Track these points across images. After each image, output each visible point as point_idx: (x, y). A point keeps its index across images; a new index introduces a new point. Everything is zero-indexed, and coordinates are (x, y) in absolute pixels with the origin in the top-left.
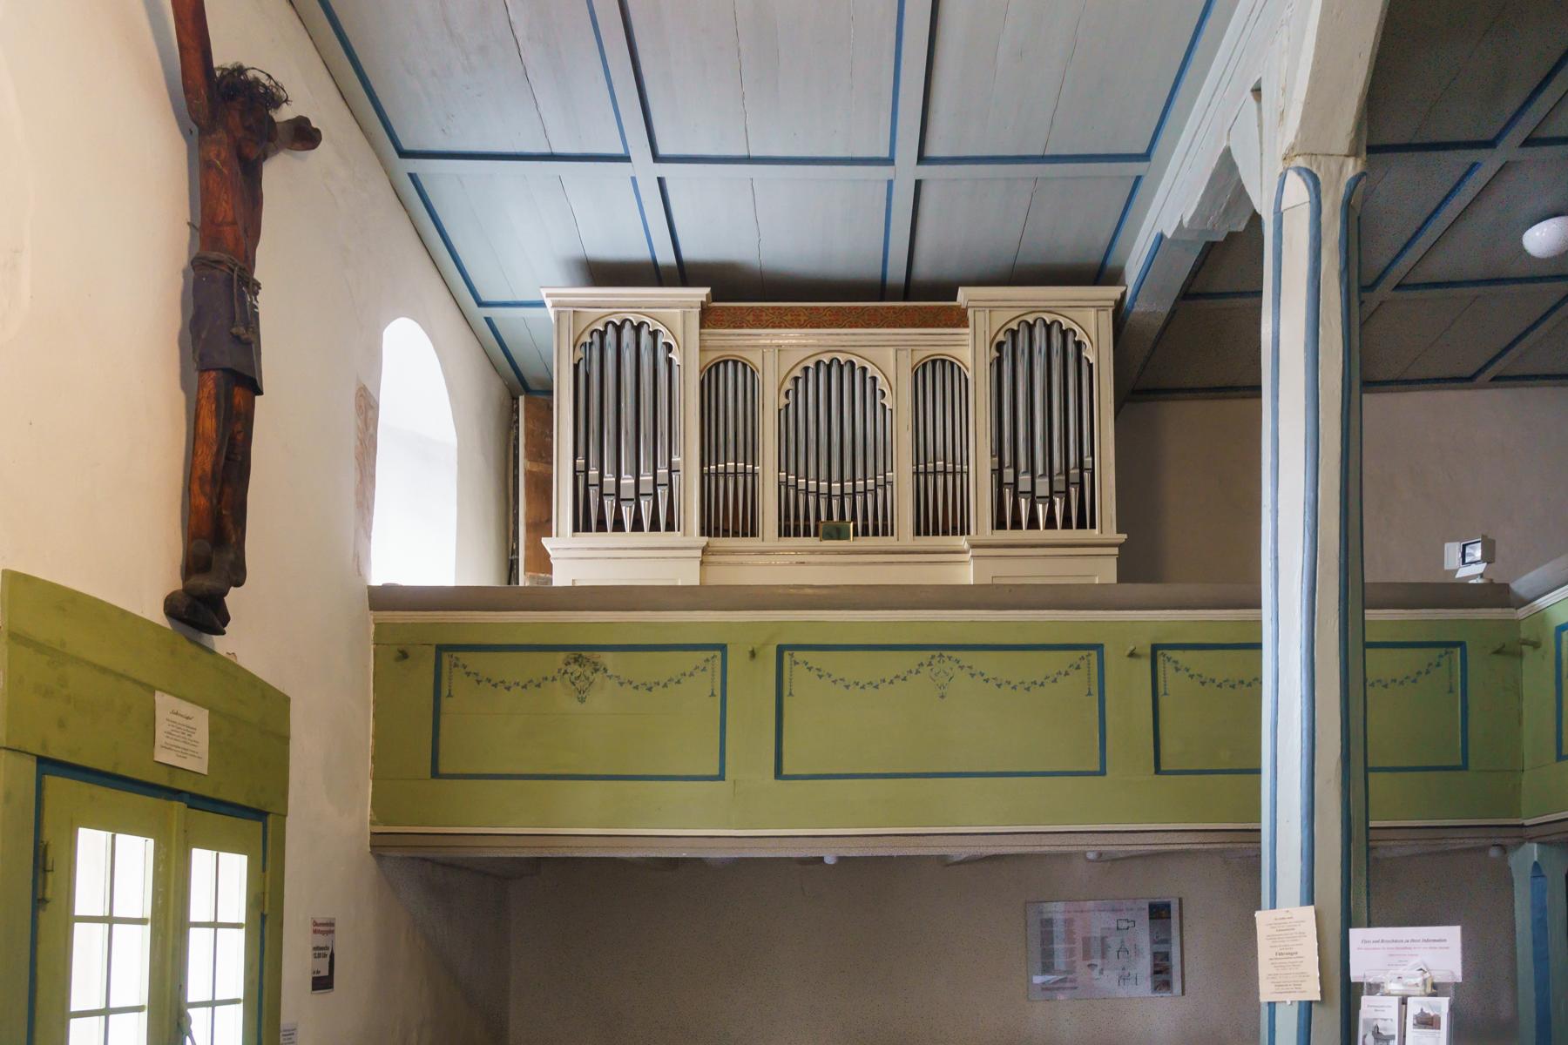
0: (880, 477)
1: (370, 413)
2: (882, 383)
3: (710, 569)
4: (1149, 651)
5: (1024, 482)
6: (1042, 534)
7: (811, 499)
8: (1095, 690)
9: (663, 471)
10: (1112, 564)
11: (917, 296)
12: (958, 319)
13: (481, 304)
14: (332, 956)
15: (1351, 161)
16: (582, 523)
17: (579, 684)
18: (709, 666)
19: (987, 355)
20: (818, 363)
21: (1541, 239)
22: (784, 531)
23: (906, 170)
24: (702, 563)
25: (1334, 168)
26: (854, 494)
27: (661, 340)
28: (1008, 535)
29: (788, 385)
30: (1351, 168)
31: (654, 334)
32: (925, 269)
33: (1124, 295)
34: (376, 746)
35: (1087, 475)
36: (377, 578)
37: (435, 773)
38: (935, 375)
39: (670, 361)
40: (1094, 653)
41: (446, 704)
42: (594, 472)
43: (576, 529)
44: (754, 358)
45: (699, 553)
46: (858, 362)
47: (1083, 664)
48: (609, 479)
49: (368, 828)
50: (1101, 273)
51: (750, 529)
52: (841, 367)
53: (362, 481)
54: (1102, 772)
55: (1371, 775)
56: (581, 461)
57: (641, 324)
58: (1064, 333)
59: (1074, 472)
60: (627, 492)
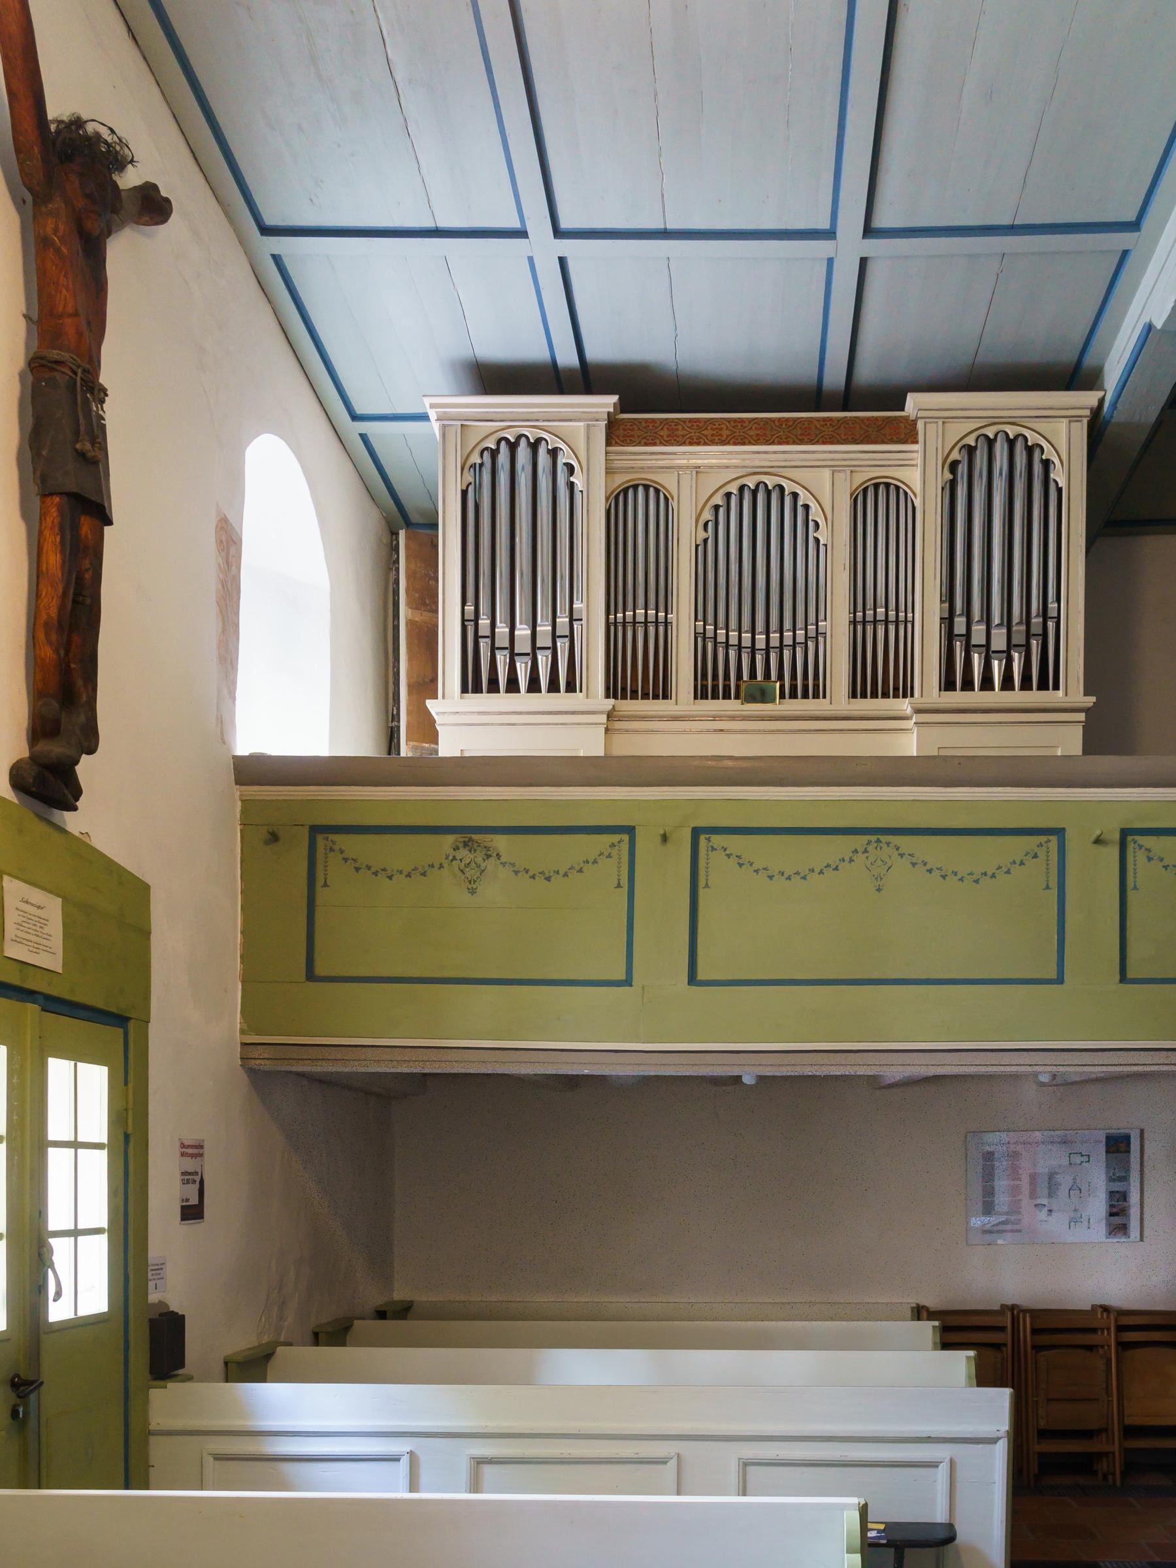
1: (232, 551)
2: (815, 513)
6: (997, 697)
7: (732, 653)
8: (1054, 883)
9: (563, 620)
11: (859, 405)
13: (355, 417)
14: (202, 1182)
16: (472, 683)
17: (470, 873)
18: (614, 852)
20: (742, 489)
22: (701, 693)
27: (561, 460)
28: (958, 697)
29: (707, 515)
33: (1101, 401)
35: (1051, 625)
36: (244, 747)
38: (877, 500)
39: (571, 486)
40: (1054, 839)
41: (322, 895)
42: (484, 622)
43: (464, 690)
44: (668, 482)
46: (789, 487)
48: (502, 629)
49: (238, 1038)
50: (1076, 375)
51: (662, 690)
54: (628, 982)
56: (470, 608)
57: (539, 440)
58: (1030, 450)
60: (523, 646)
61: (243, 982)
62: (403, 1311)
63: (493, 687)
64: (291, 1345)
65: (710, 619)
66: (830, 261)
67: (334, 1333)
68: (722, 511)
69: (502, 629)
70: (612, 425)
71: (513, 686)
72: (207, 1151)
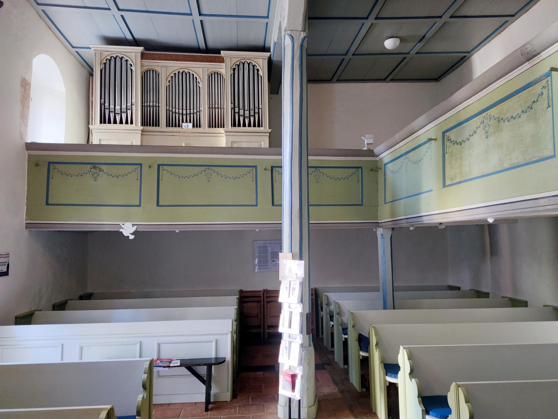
0: (198, 109)
1: (27, 87)
2: (198, 80)
3: (144, 136)
4: (270, 168)
5: (242, 112)
6: (247, 129)
7: (177, 115)
8: (254, 180)
9: (129, 104)
10: (267, 139)
11: (210, 53)
12: (221, 60)
13: (73, 47)
14: (8, 265)
15: (302, 33)
16: (103, 120)
17: (95, 175)
18: (136, 170)
19: (230, 72)
20: (179, 72)
21: (389, 44)
22: (168, 125)
23: (197, 18)
24: (142, 135)
25: (298, 35)
26: (190, 114)
27: (129, 63)
28: (237, 129)
29: (169, 79)
30: (303, 35)
31: (127, 61)
32: (211, 44)
33: (271, 55)
34: (28, 195)
35: (260, 110)
36: (30, 139)
37: (47, 204)
38: (214, 77)
39: (132, 70)
40: (254, 168)
41: (51, 181)
42: (107, 104)
43: (101, 123)
44: (158, 69)
45: (140, 132)
46: (191, 72)
47: (251, 172)
48: (112, 106)
49: (25, 222)
50: (264, 49)
51: (157, 124)
52: (186, 74)
53: (23, 109)
54: (140, 206)
55: (310, 207)
56: (103, 100)
57: (122, 57)
58: (254, 66)
59: (256, 110)
60: (118, 111)
61: (27, 205)
62: (88, 297)
63: (109, 122)
64: (41, 310)
65: (171, 106)
66: (193, 20)
67: (61, 306)
68: (174, 78)
69: (112, 106)
70: (142, 54)
71: (115, 122)
72: (10, 255)
